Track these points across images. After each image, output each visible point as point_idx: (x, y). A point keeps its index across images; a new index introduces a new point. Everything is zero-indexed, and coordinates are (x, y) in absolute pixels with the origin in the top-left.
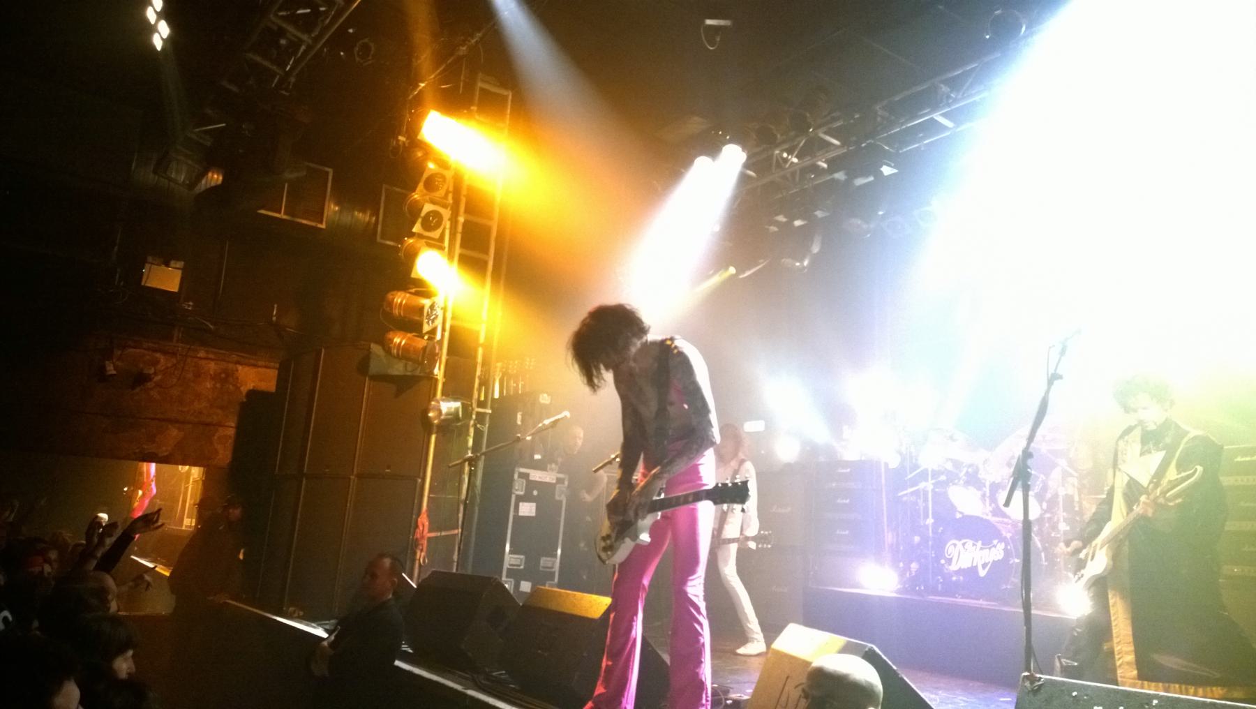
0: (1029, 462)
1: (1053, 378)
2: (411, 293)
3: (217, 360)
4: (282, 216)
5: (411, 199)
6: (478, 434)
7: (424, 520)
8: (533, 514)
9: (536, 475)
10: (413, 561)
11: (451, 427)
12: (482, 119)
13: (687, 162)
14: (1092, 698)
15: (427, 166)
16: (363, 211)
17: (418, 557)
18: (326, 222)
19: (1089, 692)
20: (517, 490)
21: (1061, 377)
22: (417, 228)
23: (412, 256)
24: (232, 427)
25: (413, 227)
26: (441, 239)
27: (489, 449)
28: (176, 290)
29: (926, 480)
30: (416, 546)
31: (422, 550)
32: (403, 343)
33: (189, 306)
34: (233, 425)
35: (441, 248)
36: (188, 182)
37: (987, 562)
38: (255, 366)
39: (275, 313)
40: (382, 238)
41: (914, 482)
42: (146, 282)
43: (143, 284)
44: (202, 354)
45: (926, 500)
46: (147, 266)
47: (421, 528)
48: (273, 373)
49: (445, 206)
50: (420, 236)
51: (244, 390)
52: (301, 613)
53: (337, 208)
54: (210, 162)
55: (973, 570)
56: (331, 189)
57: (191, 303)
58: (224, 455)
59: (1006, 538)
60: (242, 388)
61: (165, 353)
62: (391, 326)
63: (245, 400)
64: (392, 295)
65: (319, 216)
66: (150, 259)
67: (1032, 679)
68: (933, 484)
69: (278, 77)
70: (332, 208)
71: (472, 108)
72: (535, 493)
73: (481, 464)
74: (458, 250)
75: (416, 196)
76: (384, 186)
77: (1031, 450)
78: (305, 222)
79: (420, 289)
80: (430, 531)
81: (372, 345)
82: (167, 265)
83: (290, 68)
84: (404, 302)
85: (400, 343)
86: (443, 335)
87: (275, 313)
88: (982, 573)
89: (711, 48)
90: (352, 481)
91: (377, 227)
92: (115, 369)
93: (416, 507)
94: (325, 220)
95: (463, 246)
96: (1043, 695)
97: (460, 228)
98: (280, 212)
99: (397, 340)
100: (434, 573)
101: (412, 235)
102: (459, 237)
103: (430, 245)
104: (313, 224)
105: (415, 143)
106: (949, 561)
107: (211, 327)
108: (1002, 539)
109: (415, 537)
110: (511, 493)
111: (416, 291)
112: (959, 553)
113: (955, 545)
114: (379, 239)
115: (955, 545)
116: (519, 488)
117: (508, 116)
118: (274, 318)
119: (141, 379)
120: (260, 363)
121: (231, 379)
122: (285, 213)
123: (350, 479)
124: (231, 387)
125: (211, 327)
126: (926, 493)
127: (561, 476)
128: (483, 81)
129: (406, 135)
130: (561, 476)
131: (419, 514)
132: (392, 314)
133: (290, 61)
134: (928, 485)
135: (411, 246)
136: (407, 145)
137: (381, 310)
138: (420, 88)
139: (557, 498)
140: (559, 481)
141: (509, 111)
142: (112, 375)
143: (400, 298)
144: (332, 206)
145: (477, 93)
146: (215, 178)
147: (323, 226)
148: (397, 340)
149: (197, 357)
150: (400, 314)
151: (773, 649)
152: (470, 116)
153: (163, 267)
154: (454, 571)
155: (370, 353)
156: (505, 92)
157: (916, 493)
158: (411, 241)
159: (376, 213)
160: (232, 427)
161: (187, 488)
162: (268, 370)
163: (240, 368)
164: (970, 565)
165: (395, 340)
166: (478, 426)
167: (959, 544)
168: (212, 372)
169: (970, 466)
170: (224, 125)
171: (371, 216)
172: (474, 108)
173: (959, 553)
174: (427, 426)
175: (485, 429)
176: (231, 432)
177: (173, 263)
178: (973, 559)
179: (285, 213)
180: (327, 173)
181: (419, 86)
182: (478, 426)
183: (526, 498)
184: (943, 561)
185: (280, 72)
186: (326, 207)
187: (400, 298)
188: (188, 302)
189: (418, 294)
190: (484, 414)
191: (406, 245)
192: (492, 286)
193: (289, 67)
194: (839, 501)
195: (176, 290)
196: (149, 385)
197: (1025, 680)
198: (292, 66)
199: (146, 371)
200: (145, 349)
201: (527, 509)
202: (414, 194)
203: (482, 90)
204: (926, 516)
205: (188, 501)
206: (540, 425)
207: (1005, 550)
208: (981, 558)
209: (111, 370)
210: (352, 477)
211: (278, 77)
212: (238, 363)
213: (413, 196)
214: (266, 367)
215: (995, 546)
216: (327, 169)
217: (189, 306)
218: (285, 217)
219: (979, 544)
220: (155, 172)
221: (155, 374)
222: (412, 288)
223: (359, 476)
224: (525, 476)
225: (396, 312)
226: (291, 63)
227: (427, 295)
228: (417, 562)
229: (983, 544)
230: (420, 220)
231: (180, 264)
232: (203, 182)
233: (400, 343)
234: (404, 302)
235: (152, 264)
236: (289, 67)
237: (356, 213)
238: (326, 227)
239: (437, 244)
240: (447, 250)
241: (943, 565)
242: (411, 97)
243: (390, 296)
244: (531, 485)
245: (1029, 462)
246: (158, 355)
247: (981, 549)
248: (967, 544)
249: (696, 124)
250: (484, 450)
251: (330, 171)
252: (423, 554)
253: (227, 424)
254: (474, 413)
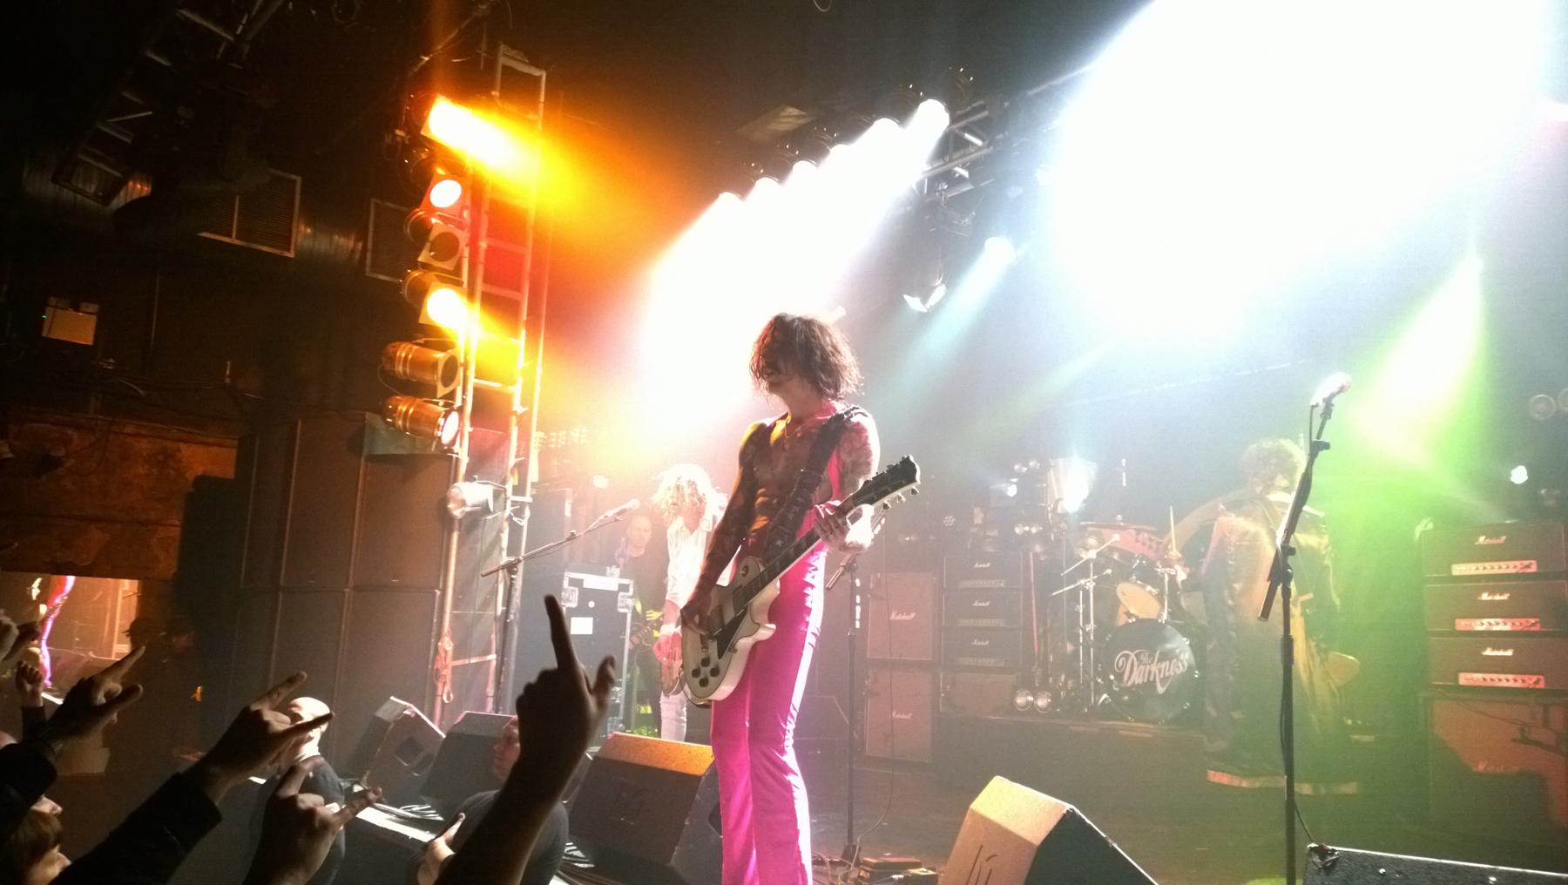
0: (1291, 560)
1: (1317, 447)
2: (417, 344)
3: (152, 436)
6: (515, 530)
7: (447, 644)
8: (590, 632)
9: (592, 581)
10: (434, 695)
11: (477, 517)
12: (512, 108)
13: (711, 196)
14: (1407, 877)
17: (439, 692)
19: (1402, 869)
21: (1326, 446)
23: (420, 293)
24: (177, 526)
25: (418, 255)
26: (457, 271)
28: (90, 343)
29: (1087, 576)
30: (437, 678)
32: (411, 411)
33: (109, 364)
35: (458, 284)
36: (101, 194)
38: (208, 444)
39: (228, 372)
40: (374, 270)
41: (1072, 578)
43: (44, 334)
44: (130, 429)
46: (49, 310)
47: (443, 655)
48: (231, 454)
49: (460, 226)
51: (190, 476)
53: (309, 231)
54: (132, 164)
56: (300, 209)
57: (111, 361)
58: (167, 564)
60: (187, 475)
63: (192, 490)
64: (394, 347)
66: (53, 301)
67: (1322, 852)
69: (224, 44)
71: (494, 93)
72: (591, 604)
77: (1292, 544)
78: (265, 249)
79: (432, 338)
80: (455, 658)
81: (368, 415)
82: (77, 309)
83: (242, 31)
84: (410, 356)
85: (407, 411)
86: (464, 400)
87: (228, 372)
89: (823, 10)
90: (347, 595)
91: (365, 258)
94: (293, 247)
95: (486, 280)
96: (1338, 875)
98: (230, 236)
99: (402, 408)
101: (415, 265)
102: (481, 269)
103: (444, 281)
105: (419, 141)
107: (142, 392)
109: (436, 667)
111: (426, 342)
115: (1127, 656)
117: (542, 106)
119: (48, 464)
120: (211, 440)
122: (237, 238)
123: (344, 593)
124: (172, 472)
125: (142, 392)
126: (1086, 593)
127: (625, 581)
129: (406, 129)
130: (625, 581)
131: (439, 636)
132: (394, 372)
133: (242, 19)
134: (1089, 584)
136: (407, 142)
137: (379, 368)
138: (423, 63)
140: (624, 588)
141: (542, 99)
143: (404, 351)
144: (303, 228)
145: (499, 75)
146: (139, 189)
147: (291, 255)
148: (402, 408)
149: (123, 434)
150: (405, 372)
152: (489, 103)
153: (71, 312)
154: (489, 709)
155: (364, 424)
156: (536, 72)
158: (416, 274)
160: (177, 526)
161: (114, 607)
163: (182, 446)
165: (400, 408)
166: (515, 519)
171: (357, 241)
172: (495, 93)
174: (446, 520)
175: (524, 523)
176: (176, 532)
177: (83, 306)
179: (237, 238)
180: (294, 182)
182: (515, 519)
186: (294, 230)
187: (404, 351)
188: (108, 358)
190: (523, 504)
193: (240, 28)
195: (90, 343)
197: (1313, 853)
199: (53, 453)
200: (53, 424)
203: (505, 68)
205: (118, 622)
206: (602, 517)
211: (224, 44)
214: (220, 446)
217: (109, 364)
218: (238, 242)
222: (420, 338)
223: (357, 588)
224: (576, 583)
226: (244, 22)
227: (444, 346)
228: (439, 700)
230: (428, 245)
231: (93, 308)
232: (122, 193)
233: (407, 411)
234: (410, 356)
235: (56, 307)
236: (240, 28)
237: (336, 237)
238: (296, 255)
239: (452, 278)
240: (465, 285)
243: (390, 349)
244: (586, 594)
245: (1291, 560)
248: (1142, 656)
249: (790, 117)
250: (523, 553)
251: (299, 179)
252: (447, 689)
253: (169, 522)
254: (509, 503)
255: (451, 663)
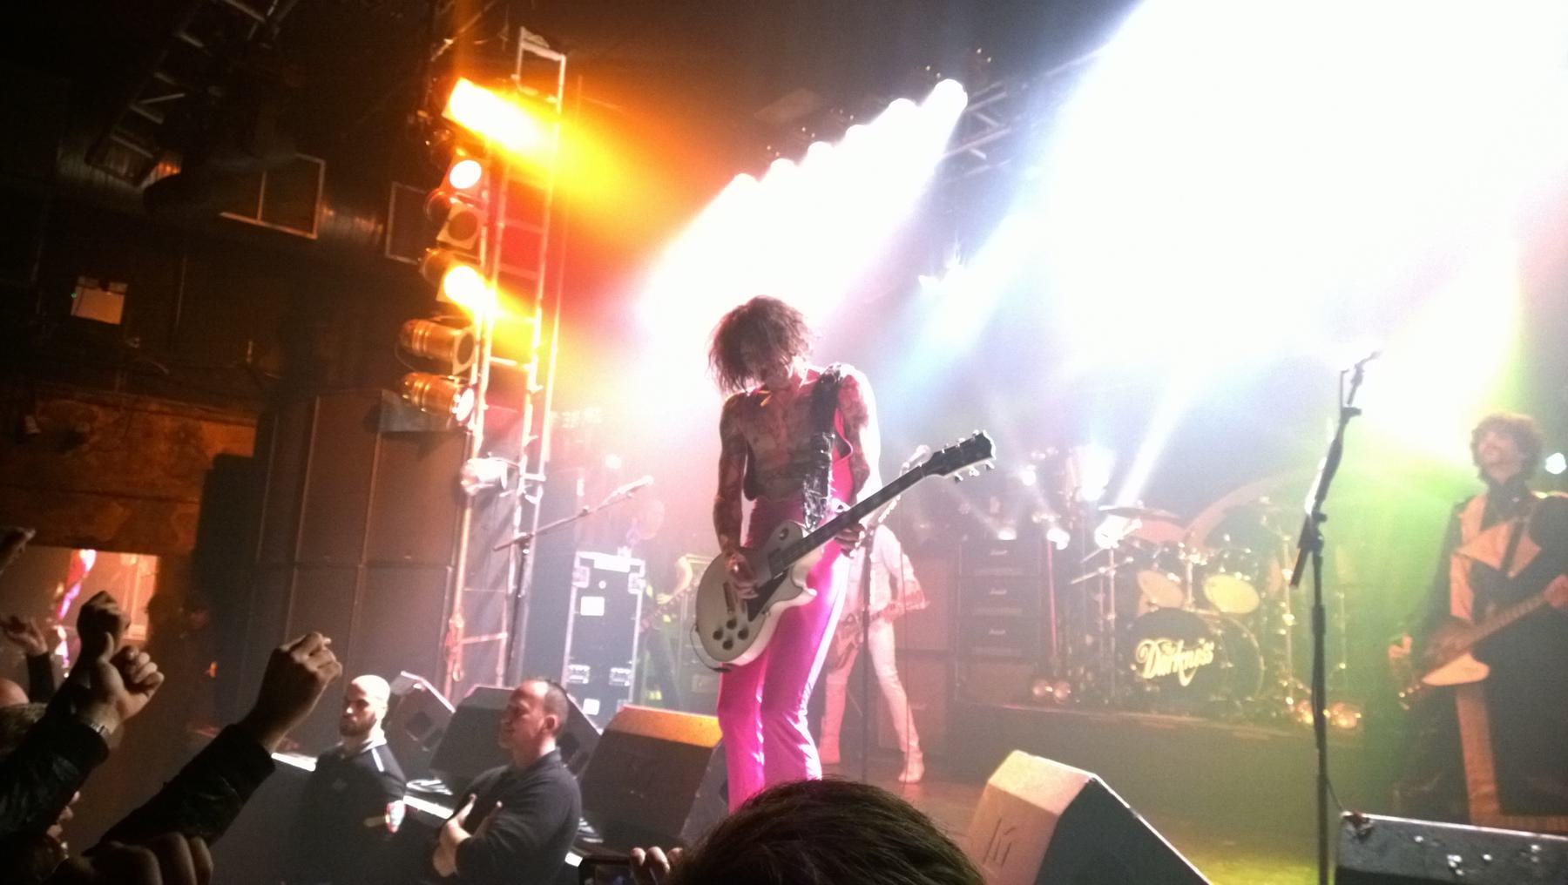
1: (1347, 414)
4: (258, 222)
5: (435, 196)
6: (527, 508)
7: (458, 622)
9: (603, 561)
15: (455, 153)
16: (367, 216)
17: (449, 670)
18: (318, 231)
20: (578, 580)
21: (1357, 412)
22: (442, 236)
23: (438, 271)
27: (543, 528)
31: (455, 662)
34: (196, 499)
35: (474, 262)
37: (1191, 666)
38: (227, 423)
40: (393, 251)
41: (1091, 566)
42: (77, 309)
44: (154, 407)
45: (1106, 590)
46: (79, 289)
50: (445, 245)
51: (211, 454)
52: (296, 746)
55: (1173, 677)
57: (137, 339)
58: (186, 540)
59: (1216, 635)
61: (104, 405)
62: (411, 367)
64: (411, 324)
65: (308, 222)
66: (82, 280)
67: (1356, 820)
68: (1116, 569)
70: (326, 214)
73: (529, 552)
74: (497, 266)
75: (440, 193)
76: (395, 185)
77: (1324, 509)
78: (289, 230)
82: (105, 288)
88: (1185, 681)
92: (39, 425)
93: (446, 606)
94: (315, 227)
96: (1374, 842)
97: (499, 237)
98: (255, 217)
99: (419, 385)
100: (479, 689)
101: (433, 244)
104: (299, 233)
105: (441, 124)
106: (1141, 667)
108: (1210, 637)
109: (446, 644)
110: (570, 586)
112: (1155, 656)
113: (1148, 646)
114: (388, 254)
116: (581, 580)
118: (249, 360)
119: (73, 439)
120: (232, 419)
121: (193, 441)
128: (527, 41)
131: (450, 614)
135: (436, 259)
138: (446, 47)
139: (631, 591)
142: (35, 435)
146: (168, 169)
147: (314, 236)
151: (990, 785)
153: (99, 292)
157: (1093, 584)
158: (435, 253)
159: (383, 219)
162: (240, 428)
163: (204, 425)
164: (1168, 672)
167: (1154, 644)
168: (166, 430)
169: (1166, 544)
170: (182, 95)
173: (1155, 656)
174: (460, 497)
176: (195, 509)
178: (1173, 663)
180: (318, 166)
181: (444, 43)
183: (592, 591)
184: (1134, 667)
185: (259, 18)
189: (444, 323)
190: (535, 483)
191: (428, 258)
192: (544, 316)
194: (993, 592)
196: (85, 447)
198: (276, 7)
201: (594, 607)
202: (437, 190)
204: (1107, 609)
207: (1215, 651)
208: (1184, 662)
209: (32, 426)
210: (361, 566)
212: (199, 418)
213: (437, 192)
214: (239, 424)
215: (1201, 647)
216: (317, 160)
218: (262, 223)
219: (1181, 644)
220: (88, 161)
221: (92, 432)
224: (587, 562)
225: (417, 346)
227: (461, 323)
229: (1185, 644)
230: (447, 225)
231: (122, 287)
235: (85, 287)
239: (471, 257)
241: (349, 716)
242: (433, 59)
243: (408, 326)
244: (597, 575)
245: (1323, 528)
246: (95, 408)
247: (1184, 650)
253: (190, 499)
255: (462, 641)
